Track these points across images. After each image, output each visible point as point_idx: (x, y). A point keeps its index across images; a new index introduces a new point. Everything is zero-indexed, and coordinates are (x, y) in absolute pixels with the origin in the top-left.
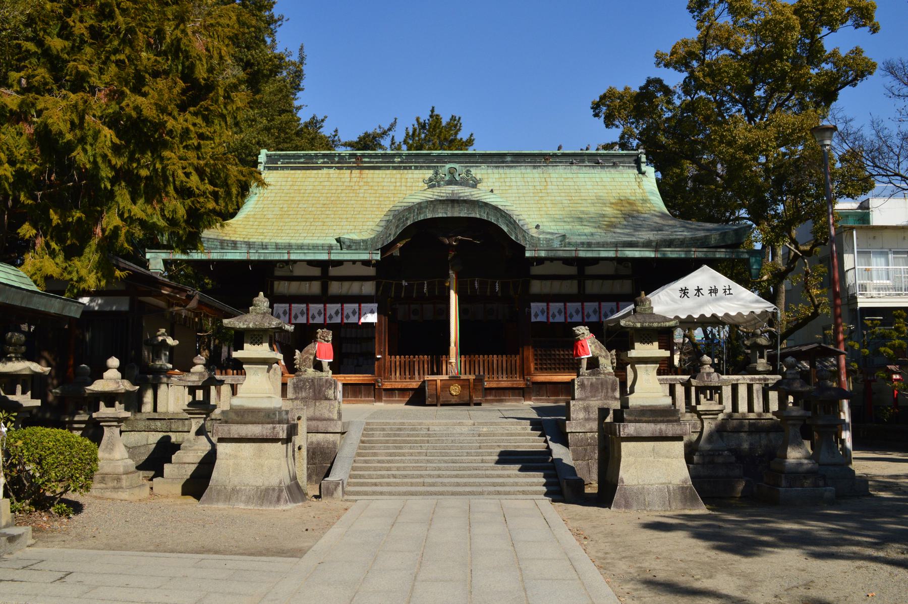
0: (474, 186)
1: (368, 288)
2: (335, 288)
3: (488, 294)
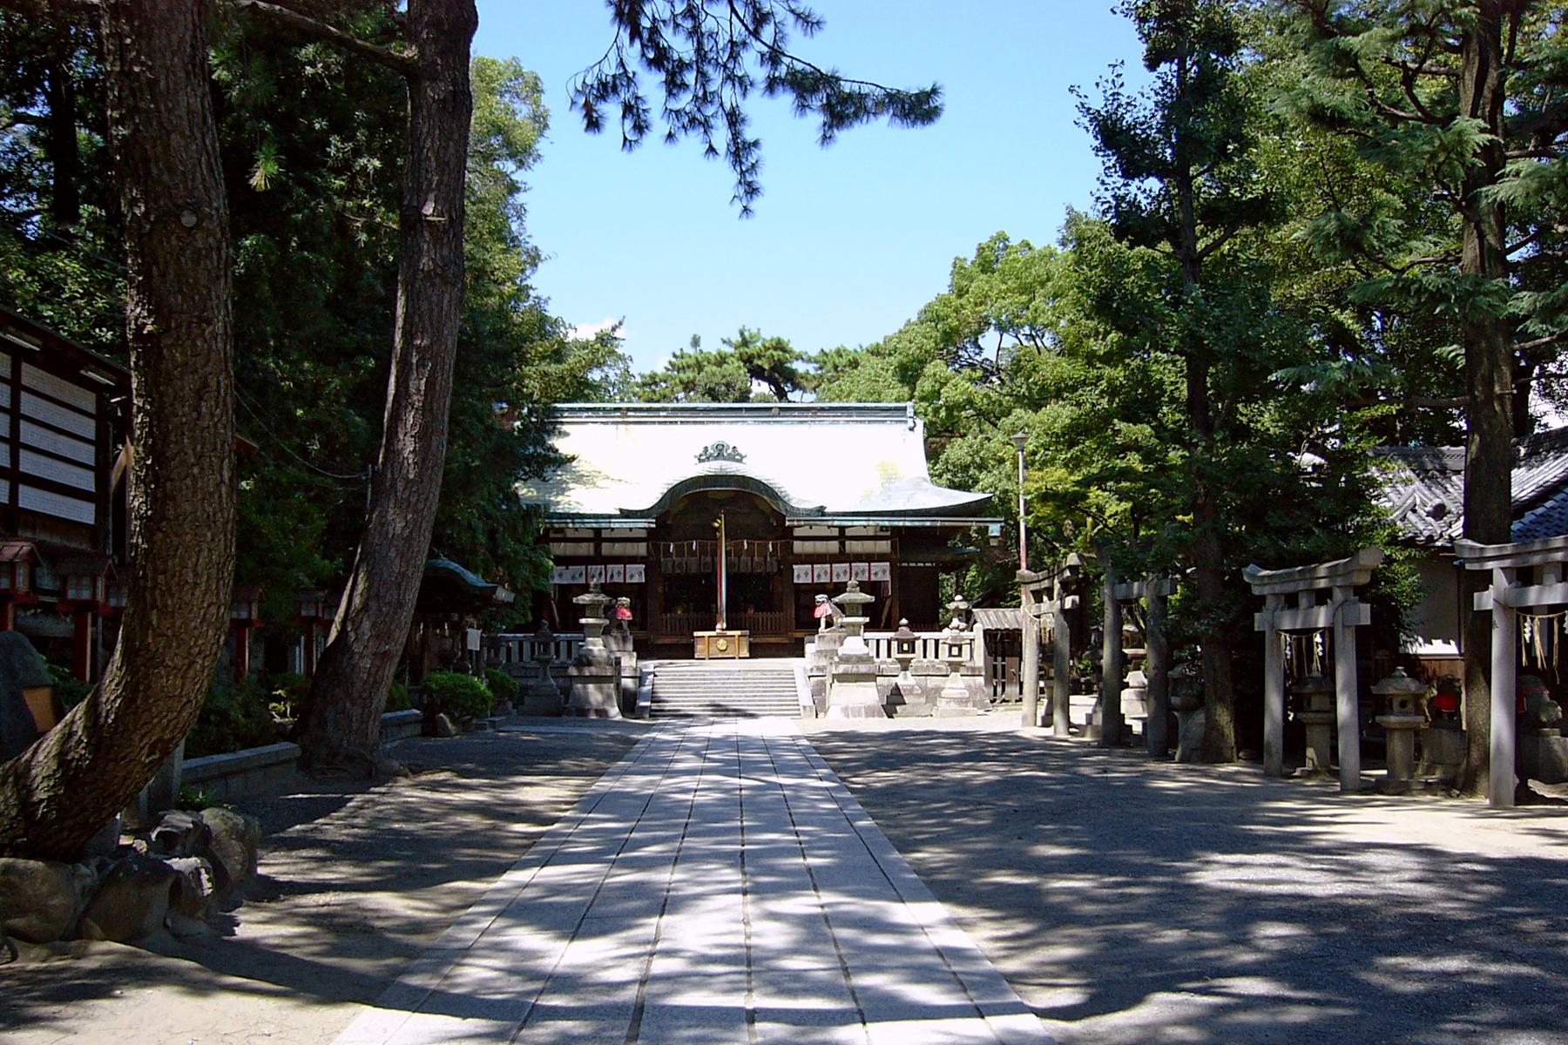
0: (740, 461)
1: (641, 549)
2: (606, 549)
3: (85, 513)
